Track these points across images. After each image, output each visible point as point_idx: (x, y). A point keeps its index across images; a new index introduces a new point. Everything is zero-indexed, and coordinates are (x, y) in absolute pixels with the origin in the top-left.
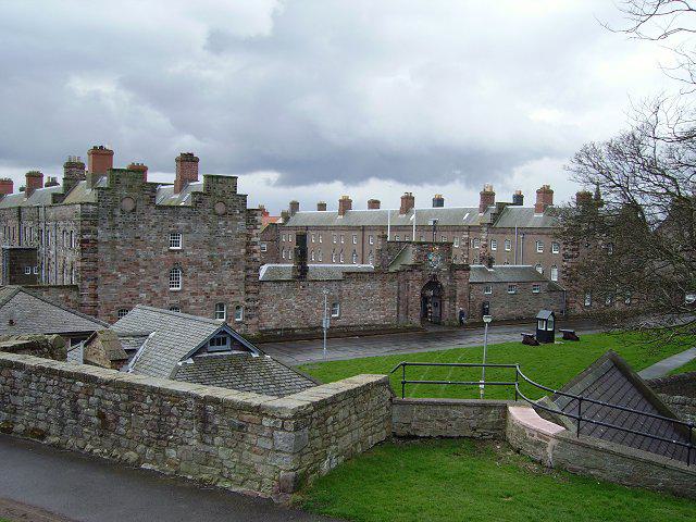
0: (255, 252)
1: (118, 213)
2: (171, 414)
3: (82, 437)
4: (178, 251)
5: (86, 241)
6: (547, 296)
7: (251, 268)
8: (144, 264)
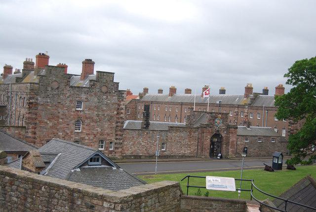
0: (122, 113)
1: (50, 89)
2: (54, 197)
3: (7, 208)
4: (81, 111)
5: (31, 103)
6: (279, 145)
7: (119, 122)
8: (62, 117)
